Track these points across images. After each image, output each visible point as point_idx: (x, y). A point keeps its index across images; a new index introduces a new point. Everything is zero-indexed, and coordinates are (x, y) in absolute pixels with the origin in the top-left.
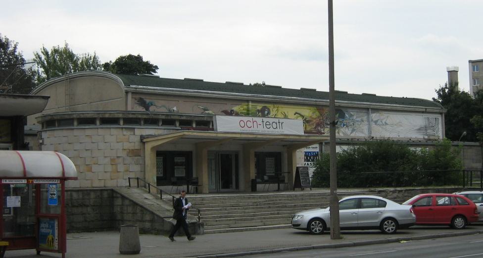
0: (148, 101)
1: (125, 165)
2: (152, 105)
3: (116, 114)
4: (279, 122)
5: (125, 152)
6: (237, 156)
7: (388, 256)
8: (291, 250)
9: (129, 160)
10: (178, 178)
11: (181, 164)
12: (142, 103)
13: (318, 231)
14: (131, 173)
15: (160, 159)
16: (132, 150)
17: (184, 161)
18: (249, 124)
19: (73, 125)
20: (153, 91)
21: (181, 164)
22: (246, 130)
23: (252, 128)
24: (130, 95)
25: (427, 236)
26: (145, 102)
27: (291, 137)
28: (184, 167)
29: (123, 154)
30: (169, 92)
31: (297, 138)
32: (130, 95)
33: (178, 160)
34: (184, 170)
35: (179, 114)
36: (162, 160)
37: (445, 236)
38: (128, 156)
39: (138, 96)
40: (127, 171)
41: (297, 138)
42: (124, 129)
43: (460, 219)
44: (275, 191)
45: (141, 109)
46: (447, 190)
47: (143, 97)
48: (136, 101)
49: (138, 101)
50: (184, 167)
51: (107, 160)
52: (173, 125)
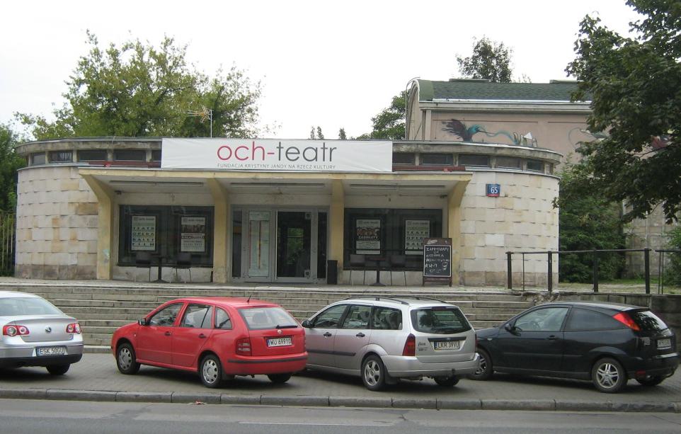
0: (468, 125)
1: (71, 230)
2: (478, 131)
3: (60, 144)
4: (324, 148)
5: (73, 208)
6: (323, 218)
7: (295, 432)
8: (329, 403)
9: (79, 220)
10: (367, 257)
11: (197, 230)
12: (457, 128)
13: (212, 363)
14: (81, 243)
15: (376, 223)
16: (84, 204)
17: (203, 223)
18: (241, 153)
19: (543, 172)
20: (474, 106)
21: (197, 230)
22: (234, 163)
23: (249, 161)
24: (429, 115)
25: (457, 403)
26: (463, 127)
27: (348, 177)
28: (203, 235)
29: (70, 211)
30: (510, 107)
31: (370, 178)
32: (429, 115)
33: (188, 222)
34: (203, 241)
35: (425, 143)
36: (428, 226)
37: (172, 400)
38: (76, 214)
39: (448, 117)
40: (74, 239)
41: (370, 178)
42: (72, 169)
43: (215, 366)
44: (155, 282)
45: (454, 139)
46: (623, 299)
47: (459, 117)
48: (445, 126)
49: (448, 126)
50: (203, 235)
51: (49, 221)
52: (539, 170)
